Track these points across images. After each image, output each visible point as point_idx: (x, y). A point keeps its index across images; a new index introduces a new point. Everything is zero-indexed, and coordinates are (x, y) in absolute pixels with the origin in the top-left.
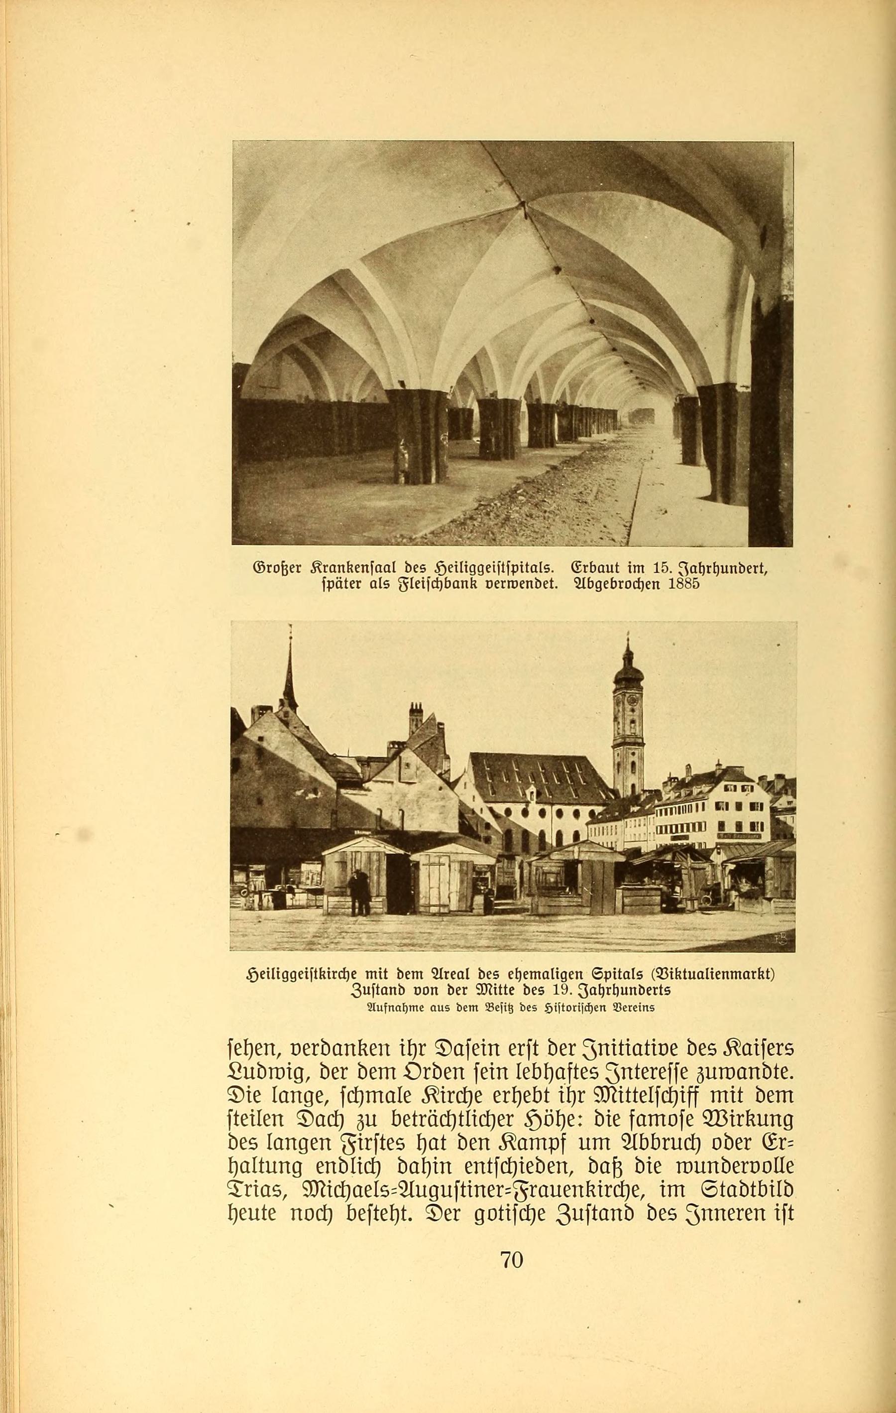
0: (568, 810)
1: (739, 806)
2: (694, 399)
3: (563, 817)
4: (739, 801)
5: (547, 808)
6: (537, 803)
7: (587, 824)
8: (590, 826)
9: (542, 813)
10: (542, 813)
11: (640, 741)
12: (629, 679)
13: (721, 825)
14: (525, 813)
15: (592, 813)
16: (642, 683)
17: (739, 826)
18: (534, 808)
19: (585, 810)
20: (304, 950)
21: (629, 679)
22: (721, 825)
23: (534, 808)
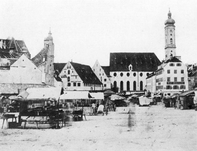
0: (118, 73)
1: (175, 72)
2: (55, 110)
3: (143, 76)
4: (180, 72)
5: (136, 73)
6: (132, 71)
7: (147, 79)
8: (147, 79)
9: (135, 75)
10: (135, 75)
11: (174, 46)
12: (170, 24)
13: (169, 79)
14: (128, 75)
15: (148, 74)
16: (175, 24)
17: (176, 79)
18: (131, 73)
19: (145, 73)
20: (49, 128)
21: (170, 24)
22: (169, 79)
23: (131, 73)
